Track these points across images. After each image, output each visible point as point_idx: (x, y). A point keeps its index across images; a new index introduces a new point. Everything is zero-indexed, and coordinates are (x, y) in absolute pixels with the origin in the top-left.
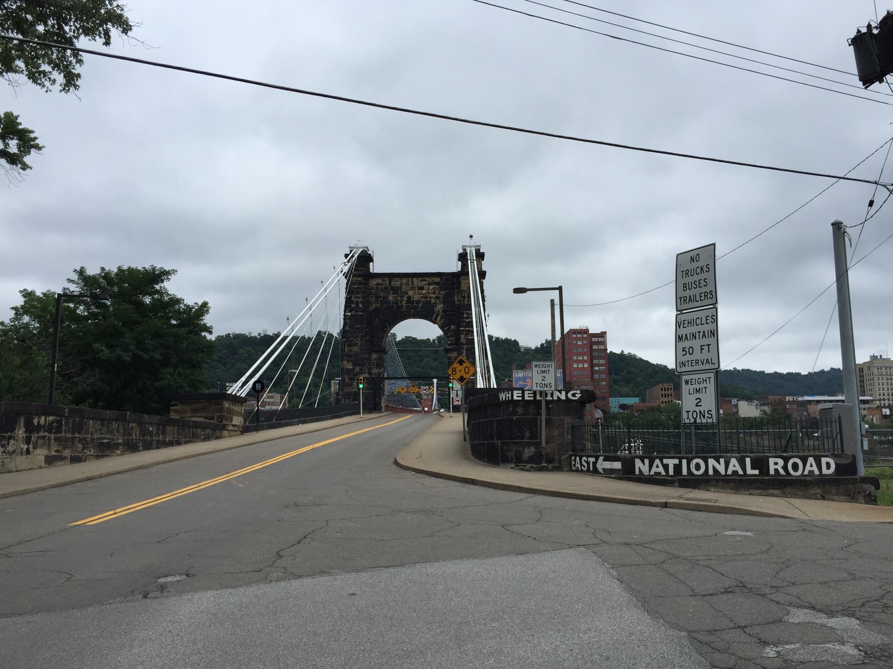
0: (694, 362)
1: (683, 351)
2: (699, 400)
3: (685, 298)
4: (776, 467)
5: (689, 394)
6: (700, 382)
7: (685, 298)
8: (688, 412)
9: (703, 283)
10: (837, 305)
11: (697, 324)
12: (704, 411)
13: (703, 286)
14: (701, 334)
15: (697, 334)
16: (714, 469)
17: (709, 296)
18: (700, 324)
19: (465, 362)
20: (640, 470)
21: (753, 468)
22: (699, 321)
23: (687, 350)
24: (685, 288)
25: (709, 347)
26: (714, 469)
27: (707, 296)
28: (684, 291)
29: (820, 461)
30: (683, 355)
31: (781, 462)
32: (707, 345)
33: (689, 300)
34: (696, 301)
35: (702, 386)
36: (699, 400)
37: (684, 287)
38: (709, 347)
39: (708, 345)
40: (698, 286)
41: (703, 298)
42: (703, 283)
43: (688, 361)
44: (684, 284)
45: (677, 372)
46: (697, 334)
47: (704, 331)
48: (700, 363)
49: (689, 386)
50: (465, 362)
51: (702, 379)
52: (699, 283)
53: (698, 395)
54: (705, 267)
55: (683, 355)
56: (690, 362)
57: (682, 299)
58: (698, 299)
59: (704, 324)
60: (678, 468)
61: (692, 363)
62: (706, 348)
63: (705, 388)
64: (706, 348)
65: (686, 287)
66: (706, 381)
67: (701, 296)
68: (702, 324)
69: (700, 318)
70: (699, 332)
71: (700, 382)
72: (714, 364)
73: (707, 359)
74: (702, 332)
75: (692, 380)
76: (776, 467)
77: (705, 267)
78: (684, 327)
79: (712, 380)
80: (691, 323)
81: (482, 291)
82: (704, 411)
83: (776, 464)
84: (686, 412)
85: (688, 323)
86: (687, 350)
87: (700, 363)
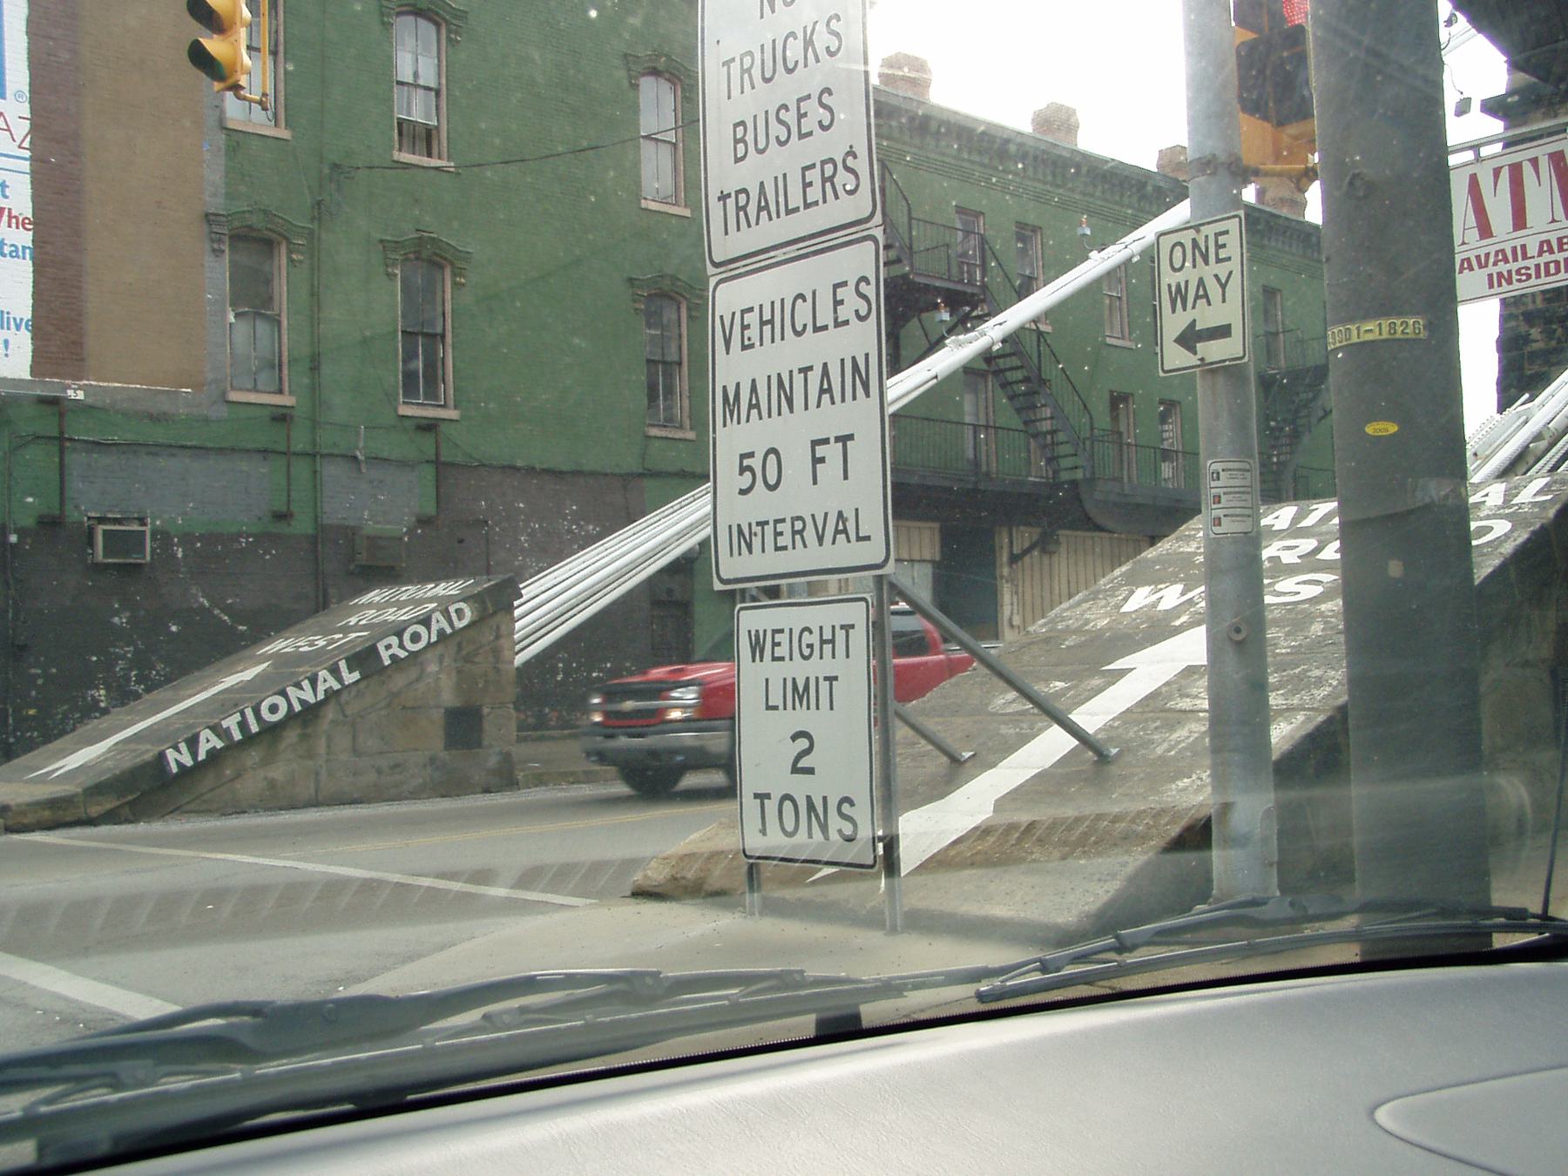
0: (785, 528)
1: (743, 470)
2: (803, 743)
3: (742, 198)
4: (390, 652)
5: (769, 708)
6: (810, 646)
7: (742, 198)
8: (762, 797)
9: (816, 113)
10: (1470, 204)
11: (799, 328)
12: (825, 799)
13: (817, 131)
14: (815, 377)
15: (798, 379)
16: (301, 701)
17: (845, 180)
18: (810, 328)
19: (1183, 594)
20: (177, 762)
21: (351, 671)
22: (803, 314)
23: (755, 462)
24: (741, 146)
25: (845, 447)
26: (301, 701)
27: (831, 179)
28: (737, 160)
29: (448, 612)
30: (743, 492)
31: (394, 640)
32: (838, 439)
33: (760, 209)
34: (788, 212)
35: (816, 668)
36: (803, 743)
37: (736, 141)
38: (845, 447)
39: (844, 439)
40: (794, 130)
41: (814, 194)
42: (816, 113)
43: (762, 524)
44: (736, 125)
45: (723, 581)
46: (798, 379)
47: (825, 365)
48: (810, 534)
49: (767, 667)
50: (1183, 594)
51: (816, 632)
52: (801, 116)
53: (801, 718)
54: (821, 27)
55: (743, 492)
56: (769, 529)
57: (731, 202)
58: (795, 200)
59: (825, 328)
60: (243, 725)
61: (778, 534)
62: (832, 452)
63: (831, 679)
64: (832, 452)
65: (743, 140)
66: (832, 641)
67: (807, 185)
68: (816, 329)
69: (809, 300)
70: (805, 370)
71: (810, 646)
72: (868, 538)
73: (840, 514)
74: (818, 370)
75: (778, 638)
76: (390, 652)
77: (821, 27)
78: (744, 348)
79: (859, 638)
80: (771, 322)
81: (815, 253)
82: (825, 799)
83: (388, 647)
84: (756, 796)
85: (763, 323)
86: (755, 462)
87: (810, 534)
